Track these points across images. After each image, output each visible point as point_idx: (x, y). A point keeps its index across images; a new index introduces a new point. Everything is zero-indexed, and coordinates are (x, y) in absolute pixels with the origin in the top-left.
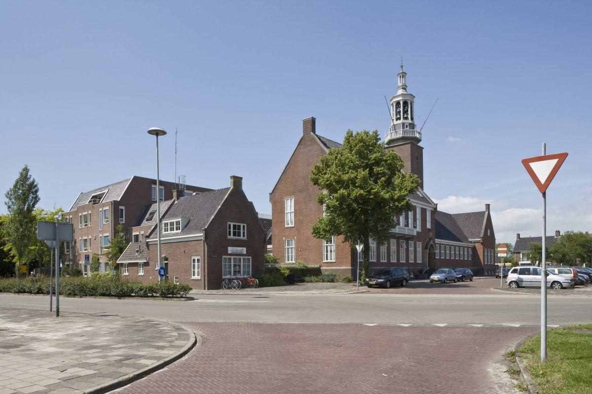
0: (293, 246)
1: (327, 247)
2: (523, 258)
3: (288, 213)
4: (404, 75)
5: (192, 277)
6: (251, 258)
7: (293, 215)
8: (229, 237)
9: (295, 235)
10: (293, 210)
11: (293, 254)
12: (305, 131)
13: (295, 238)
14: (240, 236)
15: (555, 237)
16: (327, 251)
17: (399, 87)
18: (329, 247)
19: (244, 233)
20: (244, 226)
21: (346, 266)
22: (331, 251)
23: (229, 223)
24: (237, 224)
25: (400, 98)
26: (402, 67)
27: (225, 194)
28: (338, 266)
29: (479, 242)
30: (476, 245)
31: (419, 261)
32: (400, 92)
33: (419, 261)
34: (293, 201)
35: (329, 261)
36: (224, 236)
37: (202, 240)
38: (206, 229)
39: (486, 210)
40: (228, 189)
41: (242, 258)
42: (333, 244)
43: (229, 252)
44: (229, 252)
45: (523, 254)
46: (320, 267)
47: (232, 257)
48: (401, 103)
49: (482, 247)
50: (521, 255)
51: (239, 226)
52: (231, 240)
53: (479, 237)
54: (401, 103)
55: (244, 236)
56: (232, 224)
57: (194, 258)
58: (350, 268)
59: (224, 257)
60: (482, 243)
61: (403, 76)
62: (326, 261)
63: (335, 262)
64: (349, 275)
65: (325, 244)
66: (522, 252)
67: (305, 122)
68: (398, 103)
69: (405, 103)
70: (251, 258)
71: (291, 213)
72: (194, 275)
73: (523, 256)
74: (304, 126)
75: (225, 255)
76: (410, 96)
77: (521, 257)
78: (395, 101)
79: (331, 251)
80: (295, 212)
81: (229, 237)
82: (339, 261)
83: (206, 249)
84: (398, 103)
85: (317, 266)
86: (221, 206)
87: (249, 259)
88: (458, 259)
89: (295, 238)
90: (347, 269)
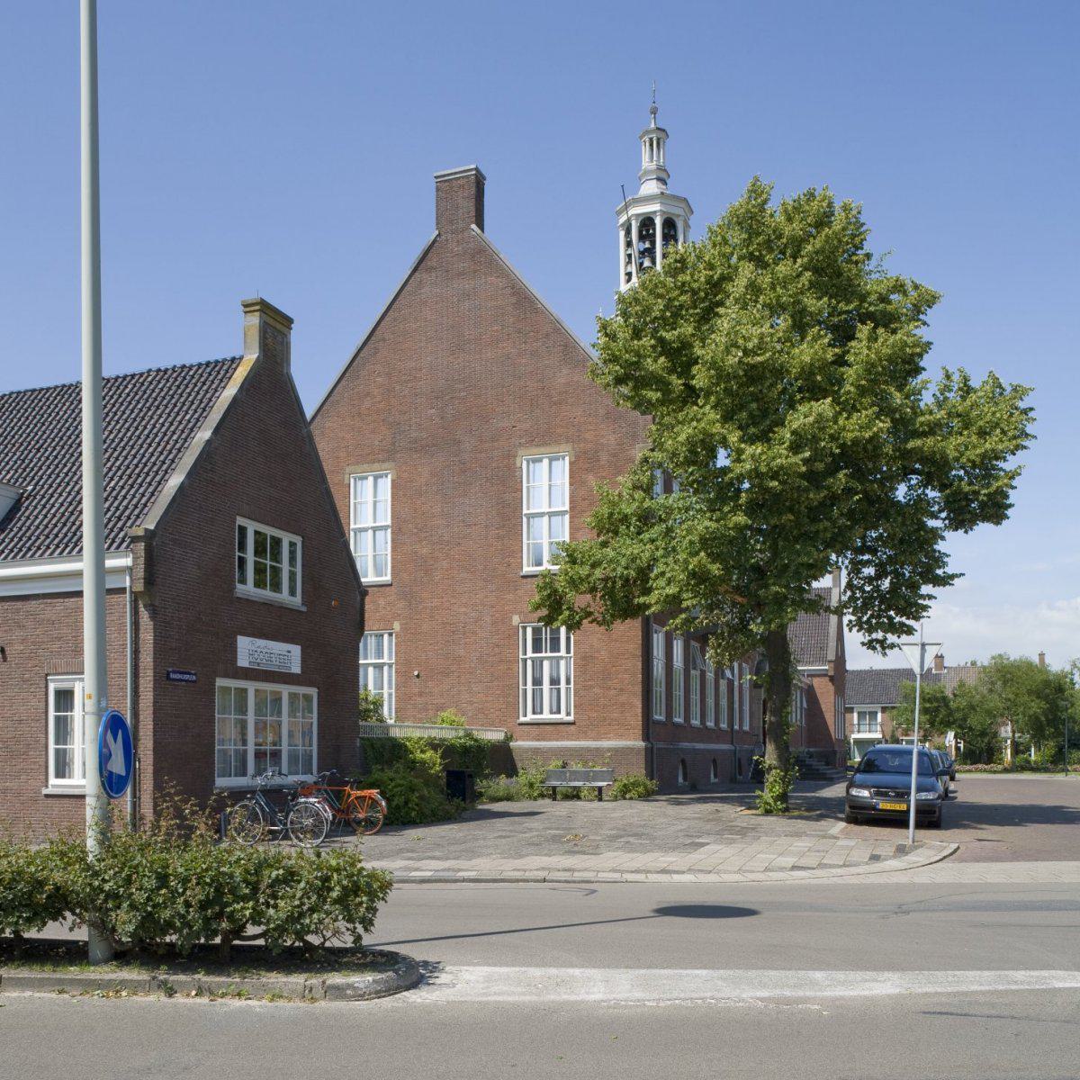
0: (386, 660)
1: (538, 665)
2: (859, 724)
3: (365, 530)
4: (660, 138)
5: (53, 781)
6: (313, 692)
7: (386, 539)
8: (239, 586)
9: (396, 617)
10: (386, 519)
11: (222, 685)
12: (444, 217)
13: (397, 626)
14: (276, 587)
15: (934, 671)
16: (537, 682)
17: (647, 172)
18: (546, 664)
19: (292, 576)
20: (292, 544)
21: (621, 736)
22: (555, 681)
23: (240, 521)
24: (270, 531)
25: (655, 207)
26: (654, 112)
27: (227, 377)
28: (586, 738)
29: (826, 675)
30: (816, 682)
31: (746, 728)
32: (651, 187)
33: (746, 728)
34: (386, 485)
35: (546, 716)
36: (224, 572)
37: (123, 590)
38: (149, 536)
39: (834, 586)
40: (222, 369)
41: (285, 690)
42: (563, 653)
43: (243, 661)
44: (243, 661)
45: (859, 713)
46: (509, 738)
47: (251, 687)
48: (658, 222)
49: (831, 688)
50: (855, 715)
51: (277, 542)
52: (248, 602)
53: (823, 660)
54: (658, 222)
55: (293, 593)
56: (252, 527)
57: (65, 686)
58: (641, 744)
59: (220, 682)
60: (832, 679)
61: (658, 140)
62: (530, 717)
63: (573, 723)
64: (638, 772)
65: (530, 654)
66: (858, 708)
67: (445, 186)
68: (647, 222)
69: (669, 224)
70: (313, 692)
71: (375, 529)
72: (60, 773)
73: (859, 717)
74: (439, 200)
75: (226, 675)
76: (683, 205)
77: (856, 722)
78: (638, 215)
79: (555, 681)
80: (398, 528)
81: (239, 586)
82: (590, 716)
83: (147, 637)
84: (647, 222)
85: (494, 736)
86: (217, 431)
87: (308, 698)
88: (662, 718)
89: (397, 626)
90: (631, 749)
